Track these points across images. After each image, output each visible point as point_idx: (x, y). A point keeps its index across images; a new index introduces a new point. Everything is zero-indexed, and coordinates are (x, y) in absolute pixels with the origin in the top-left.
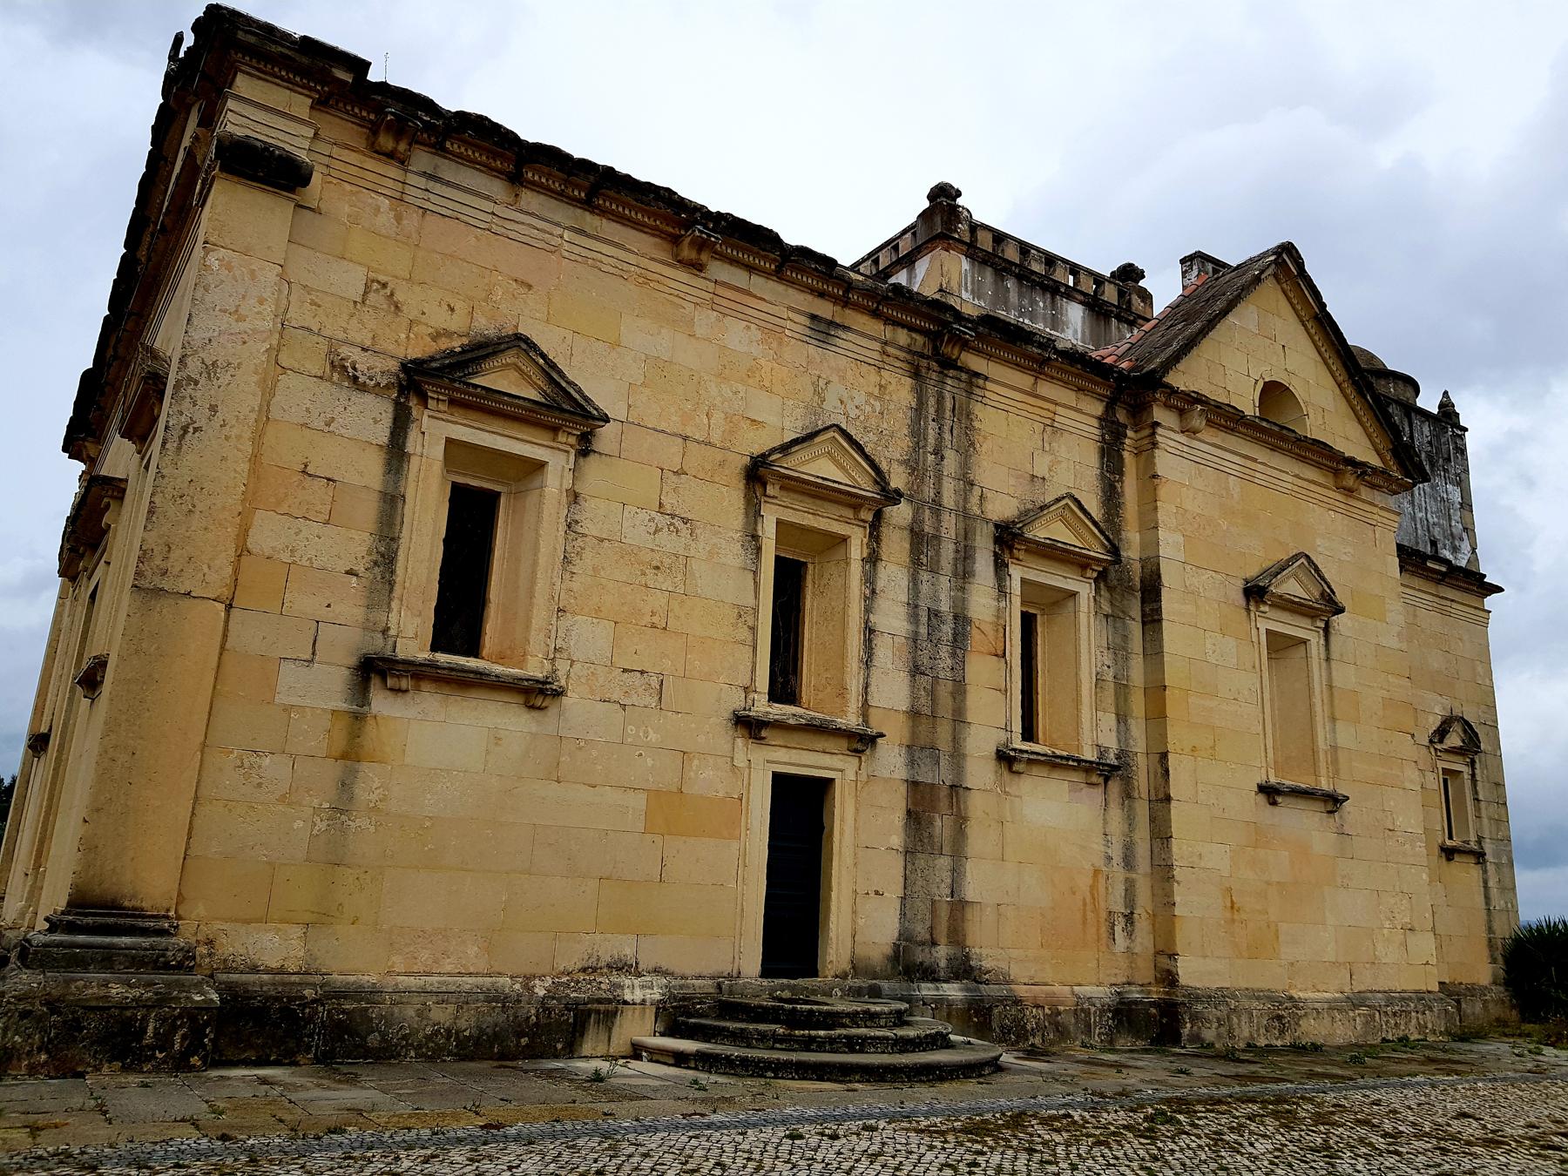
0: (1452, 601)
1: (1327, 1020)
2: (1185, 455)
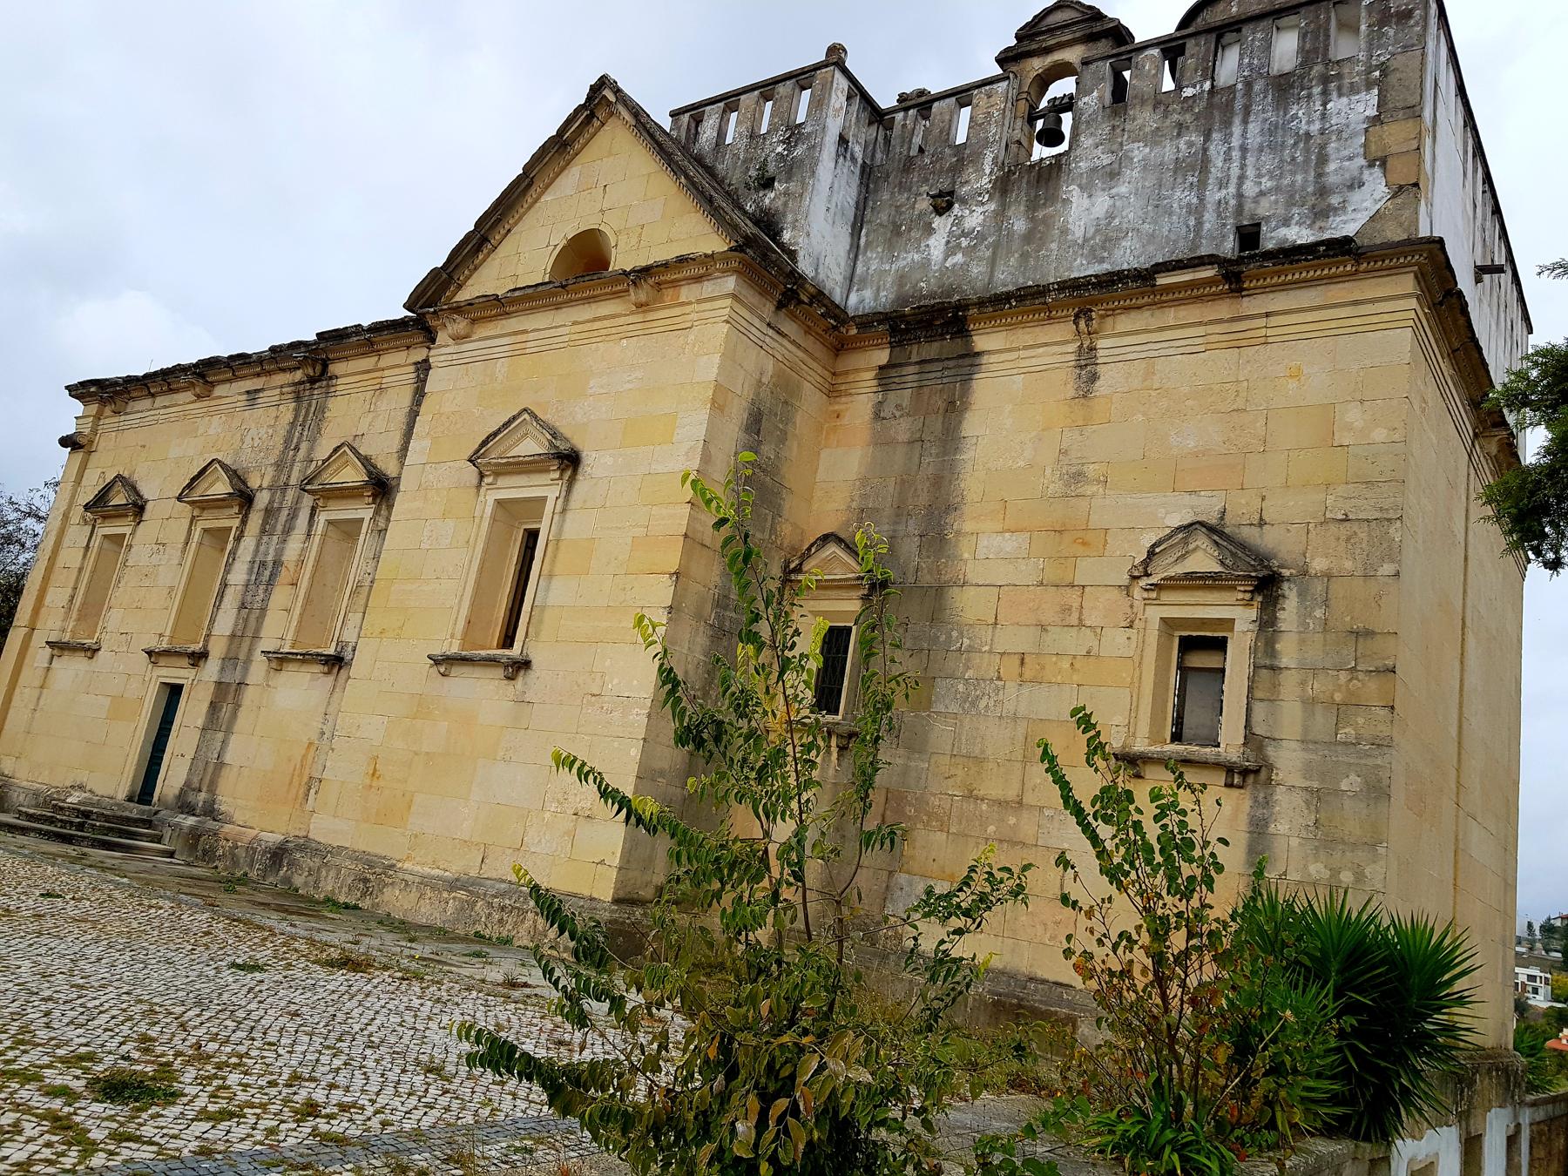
0: (1267, 315)
1: (414, 895)
2: (454, 362)
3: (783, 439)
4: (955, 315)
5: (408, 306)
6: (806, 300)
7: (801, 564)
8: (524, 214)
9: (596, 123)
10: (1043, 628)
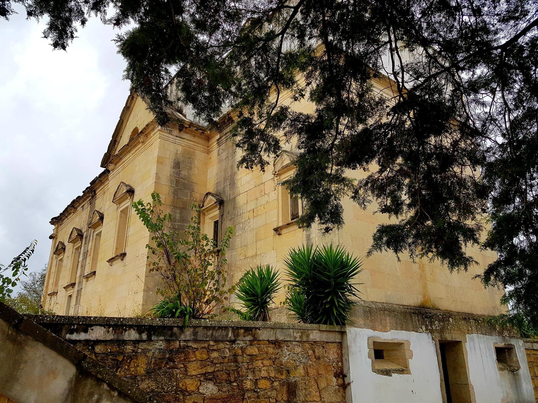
3: (190, 168)
4: (229, 117)
5: (102, 166)
6: (187, 126)
7: (203, 205)
8: (124, 130)
9: (135, 99)
10: (257, 199)
